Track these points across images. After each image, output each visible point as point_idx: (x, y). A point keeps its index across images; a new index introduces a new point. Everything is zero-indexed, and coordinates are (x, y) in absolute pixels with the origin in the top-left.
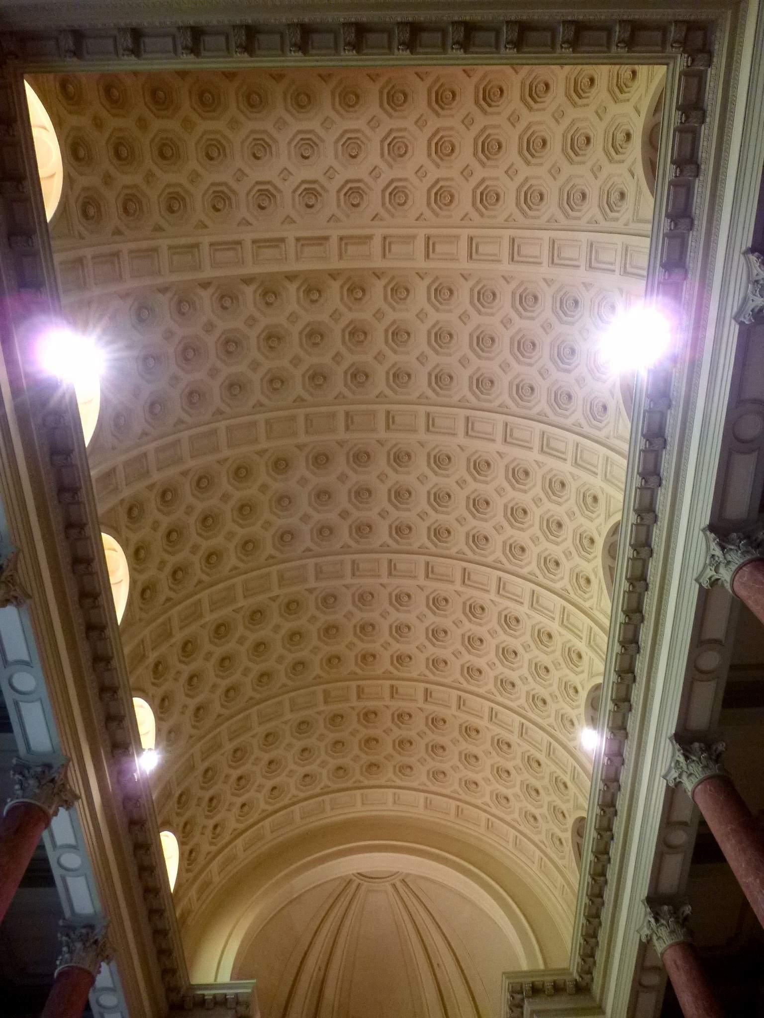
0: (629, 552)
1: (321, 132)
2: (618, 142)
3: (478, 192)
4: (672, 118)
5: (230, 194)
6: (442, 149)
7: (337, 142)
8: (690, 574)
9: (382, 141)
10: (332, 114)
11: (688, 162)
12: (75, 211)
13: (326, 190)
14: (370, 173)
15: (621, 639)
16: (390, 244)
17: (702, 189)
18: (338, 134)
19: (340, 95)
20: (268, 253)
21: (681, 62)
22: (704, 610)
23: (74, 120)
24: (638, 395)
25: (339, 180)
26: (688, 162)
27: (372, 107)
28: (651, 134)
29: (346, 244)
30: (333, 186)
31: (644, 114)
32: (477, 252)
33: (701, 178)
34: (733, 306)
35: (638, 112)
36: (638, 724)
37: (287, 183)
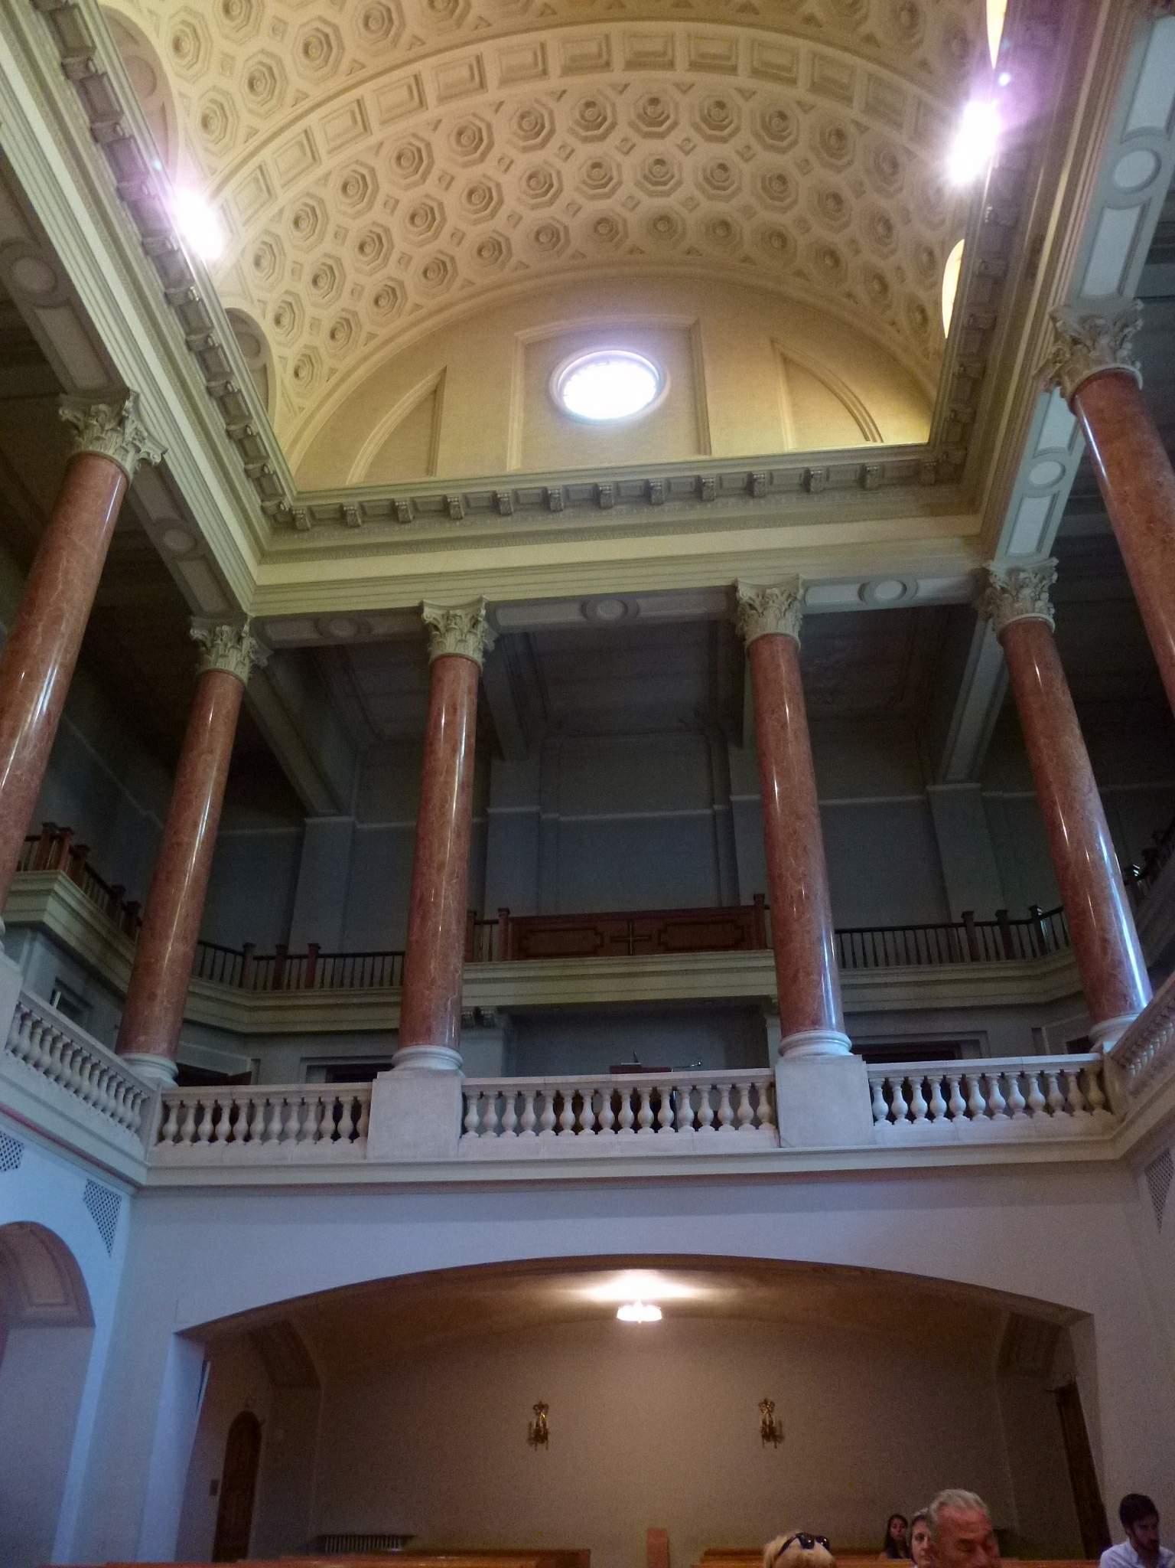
0: (237, 383)
1: (640, 195)
2: (268, 256)
3: (396, 22)
4: (242, 382)
5: (763, 133)
6: (483, 197)
7: (620, 183)
8: (149, 395)
9: (560, 190)
10: (627, 214)
11: (206, 354)
12: (930, 312)
13: (632, 124)
14: (573, 151)
15: (133, 145)
16: (536, 64)
17: (174, 331)
18: (619, 192)
19: (617, 233)
20: (713, 48)
21: (288, 502)
22: (92, 346)
23: (922, 295)
24: (151, 147)
25: (614, 139)
26: (206, 354)
27: (576, 225)
28: (155, 78)
29: (600, 55)
30: (623, 130)
31: (276, 359)
32: (410, 88)
33: (203, 388)
34: (147, 402)
35: (181, 94)
36: (184, 372)
37: (684, 136)
